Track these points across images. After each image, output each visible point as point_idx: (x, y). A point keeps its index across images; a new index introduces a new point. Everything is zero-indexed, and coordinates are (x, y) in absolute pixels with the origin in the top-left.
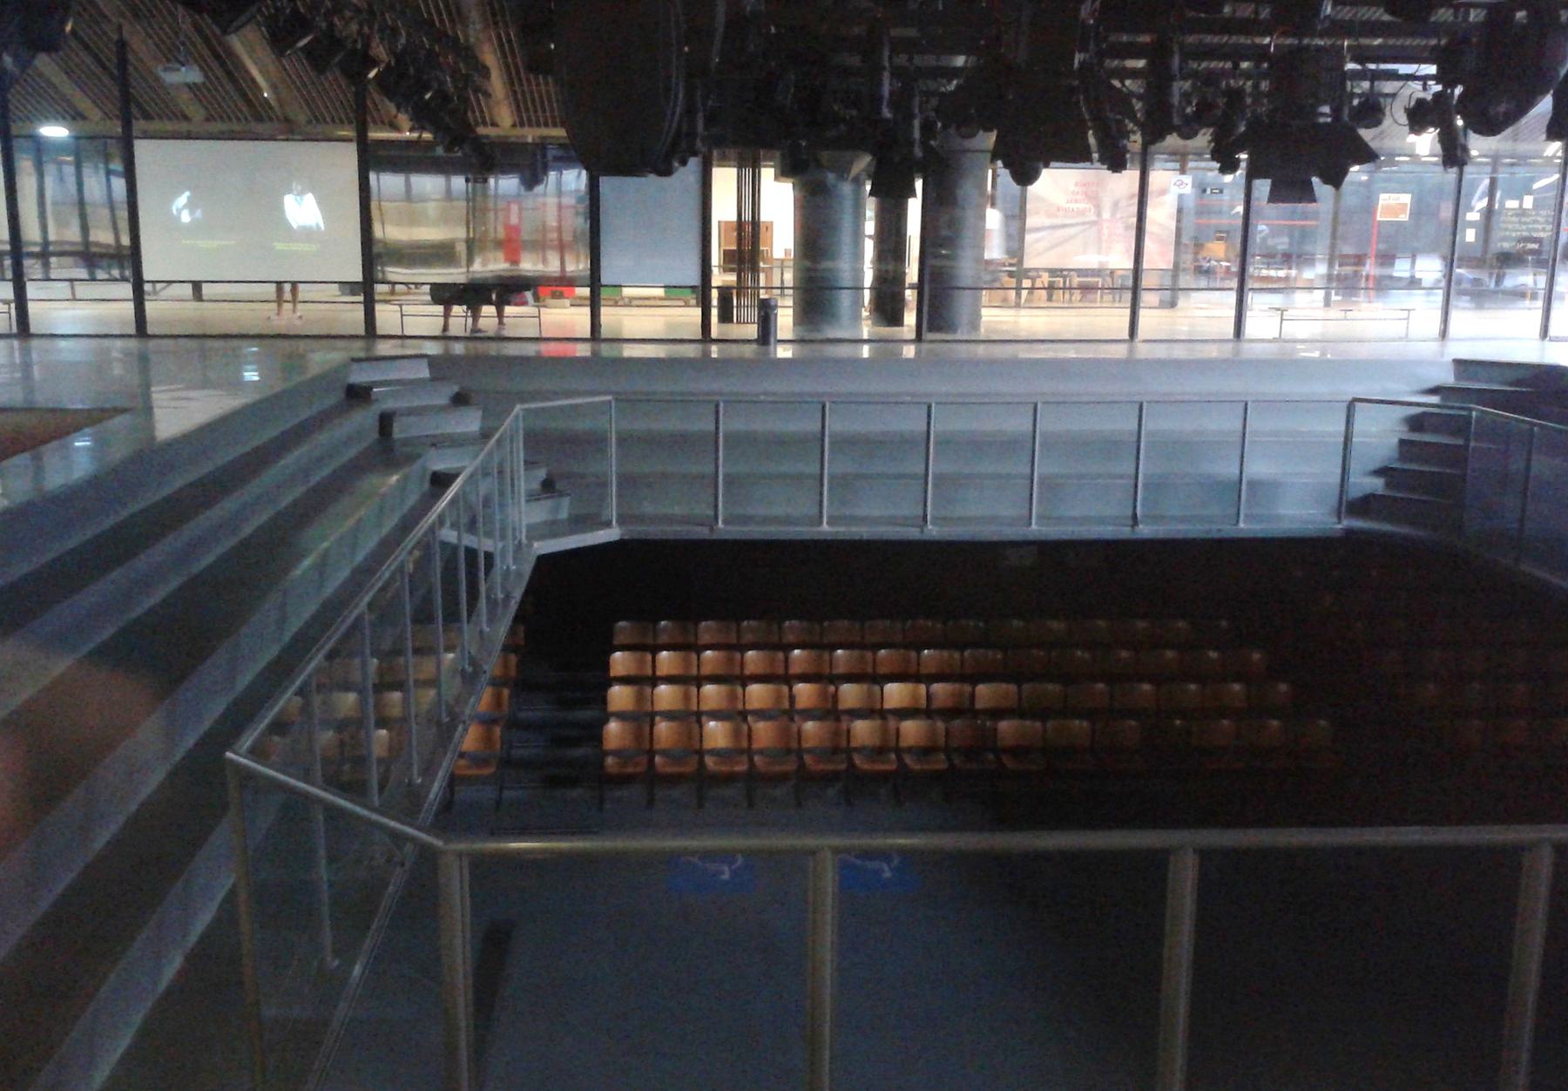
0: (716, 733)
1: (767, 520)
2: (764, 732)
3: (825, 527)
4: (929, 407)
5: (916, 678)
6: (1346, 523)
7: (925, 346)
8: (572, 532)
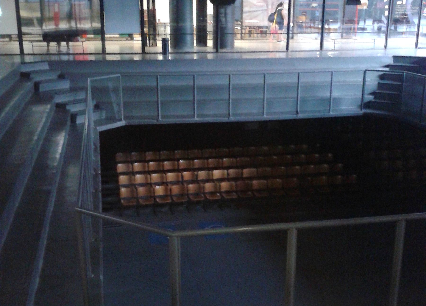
0: (159, 190)
1: (174, 117)
2: (175, 189)
3: (196, 118)
4: (230, 76)
5: (223, 168)
6: (364, 111)
7: (219, 54)
8: (107, 123)
